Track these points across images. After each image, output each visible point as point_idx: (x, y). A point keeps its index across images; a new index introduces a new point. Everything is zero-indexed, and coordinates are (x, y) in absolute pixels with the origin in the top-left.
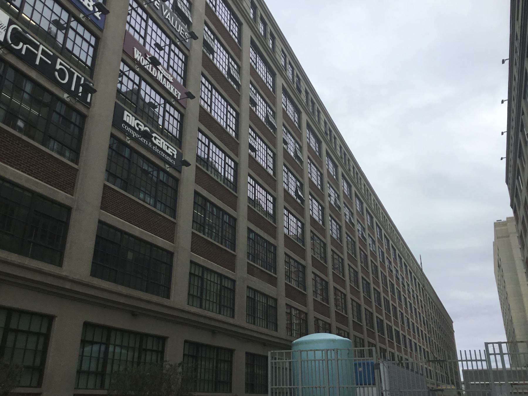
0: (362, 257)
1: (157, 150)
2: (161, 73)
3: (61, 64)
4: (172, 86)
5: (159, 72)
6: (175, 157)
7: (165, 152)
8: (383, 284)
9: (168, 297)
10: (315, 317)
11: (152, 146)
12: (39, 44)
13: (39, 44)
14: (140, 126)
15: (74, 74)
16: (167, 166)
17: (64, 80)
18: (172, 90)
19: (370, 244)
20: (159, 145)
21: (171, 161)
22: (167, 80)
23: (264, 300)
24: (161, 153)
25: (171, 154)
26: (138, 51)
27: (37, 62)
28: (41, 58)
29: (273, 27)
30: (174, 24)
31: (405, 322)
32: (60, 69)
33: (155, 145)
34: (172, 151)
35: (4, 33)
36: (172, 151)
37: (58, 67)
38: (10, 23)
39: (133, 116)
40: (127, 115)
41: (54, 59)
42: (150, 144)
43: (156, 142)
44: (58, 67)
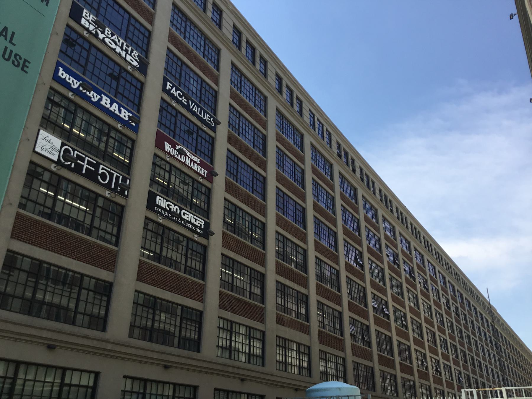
0: (426, 307)
1: (186, 224)
2: (189, 157)
3: (103, 169)
4: (199, 167)
5: (187, 157)
6: (203, 227)
7: (193, 224)
8: (458, 337)
9: (199, 351)
10: (380, 370)
11: (181, 221)
12: (84, 156)
13: (84, 156)
14: (170, 207)
15: (113, 174)
16: (196, 236)
17: (105, 181)
18: (199, 171)
19: (444, 303)
20: (187, 219)
21: (199, 231)
22: (195, 162)
23: (281, 342)
24: (189, 226)
25: (199, 225)
26: (168, 144)
27: (84, 172)
28: (86, 167)
29: (289, 80)
30: (200, 114)
31: (490, 372)
32: (103, 173)
33: (184, 219)
34: (199, 222)
35: (58, 154)
36: (200, 222)
37: (101, 171)
38: (63, 145)
39: (164, 198)
40: (159, 199)
41: (97, 166)
42: (180, 219)
43: (185, 217)
44: (101, 171)
